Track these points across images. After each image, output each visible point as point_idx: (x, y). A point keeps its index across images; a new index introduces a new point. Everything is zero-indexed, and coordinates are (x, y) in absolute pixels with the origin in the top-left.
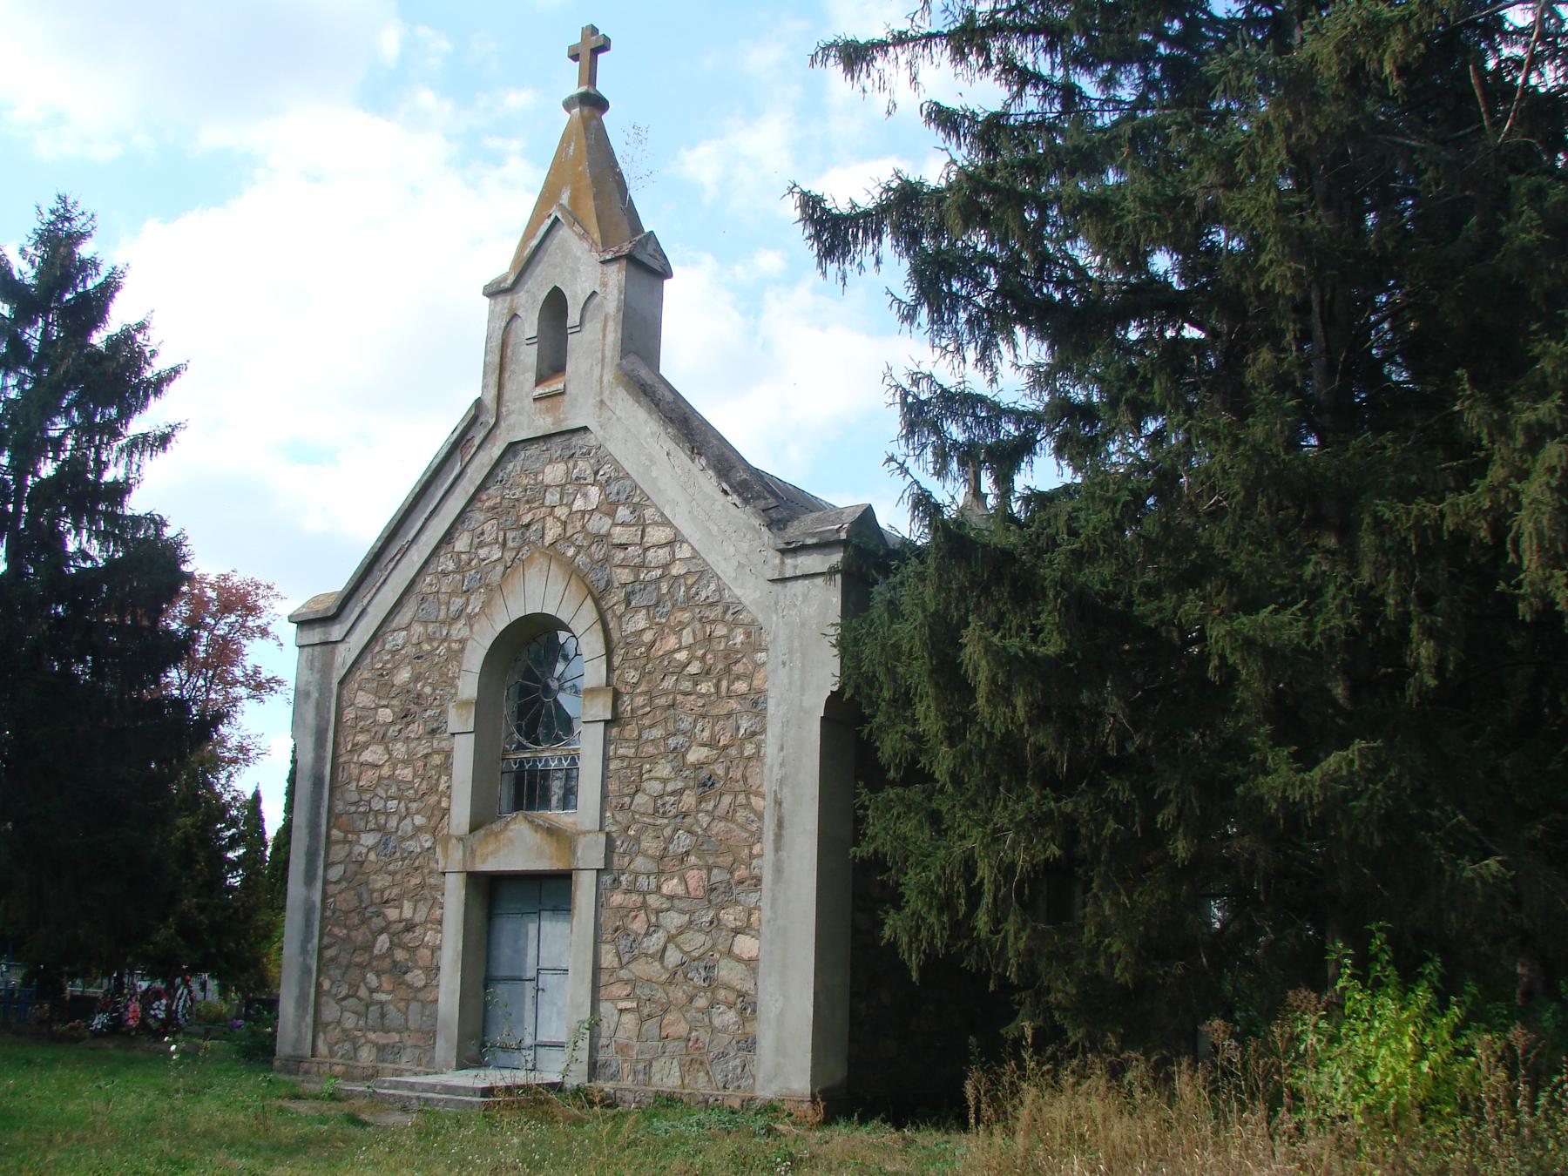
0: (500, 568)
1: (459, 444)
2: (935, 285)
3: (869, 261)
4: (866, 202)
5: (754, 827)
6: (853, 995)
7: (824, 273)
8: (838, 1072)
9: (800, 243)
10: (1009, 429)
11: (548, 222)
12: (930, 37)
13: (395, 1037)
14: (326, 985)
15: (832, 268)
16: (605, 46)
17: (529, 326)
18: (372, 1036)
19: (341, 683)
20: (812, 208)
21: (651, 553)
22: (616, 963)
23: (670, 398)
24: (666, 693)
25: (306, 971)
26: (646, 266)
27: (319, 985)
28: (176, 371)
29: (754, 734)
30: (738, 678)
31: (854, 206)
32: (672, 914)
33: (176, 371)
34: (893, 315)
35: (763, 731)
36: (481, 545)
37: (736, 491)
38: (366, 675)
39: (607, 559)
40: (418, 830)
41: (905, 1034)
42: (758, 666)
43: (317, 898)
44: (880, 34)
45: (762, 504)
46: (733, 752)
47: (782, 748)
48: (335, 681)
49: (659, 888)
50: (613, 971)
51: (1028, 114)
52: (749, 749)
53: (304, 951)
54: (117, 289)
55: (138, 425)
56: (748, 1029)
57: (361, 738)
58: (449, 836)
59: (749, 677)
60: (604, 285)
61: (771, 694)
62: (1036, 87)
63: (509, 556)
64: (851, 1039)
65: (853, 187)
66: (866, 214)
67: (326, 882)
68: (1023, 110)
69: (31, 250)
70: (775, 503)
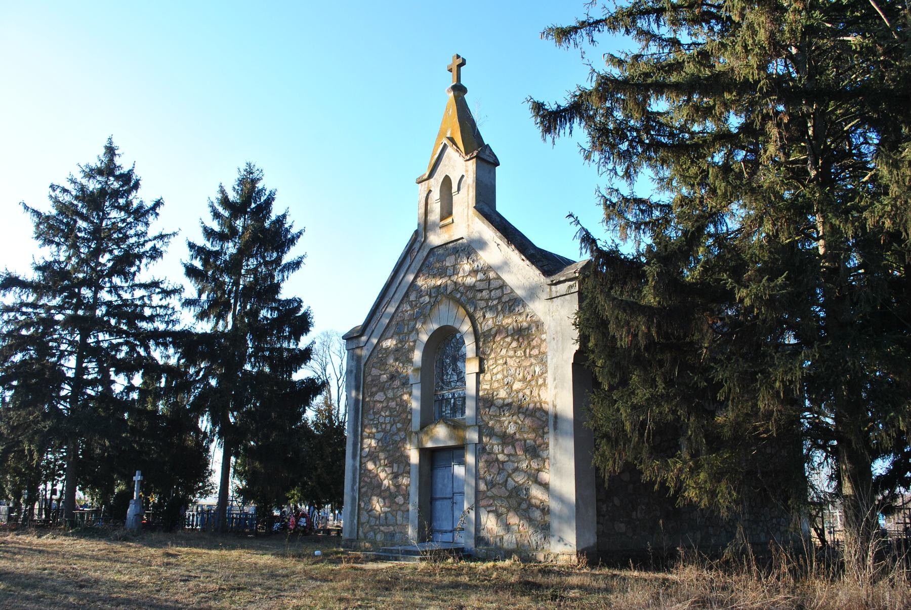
0: (429, 306)
1: (409, 250)
2: (606, 139)
3: (568, 131)
4: (564, 104)
5: (544, 419)
6: (597, 501)
7: (545, 140)
8: (591, 540)
9: (532, 126)
10: (657, 213)
11: (441, 146)
12: (597, 22)
13: (392, 528)
14: (362, 505)
15: (549, 137)
16: (463, 63)
17: (436, 195)
18: (382, 528)
19: (365, 365)
20: (538, 107)
21: (493, 293)
22: (485, 489)
23: (498, 219)
24: (502, 357)
25: (353, 499)
26: (486, 161)
27: (359, 505)
28: (300, 233)
29: (542, 374)
30: (534, 347)
31: (559, 106)
32: (510, 463)
33: (300, 233)
34: (581, 157)
35: (546, 372)
36: (421, 297)
37: (528, 258)
38: (375, 360)
39: (474, 297)
40: (399, 430)
41: (630, 521)
42: (543, 341)
43: (358, 464)
44: (574, 24)
45: (540, 264)
46: (533, 383)
47: (555, 380)
48: (362, 365)
49: (503, 451)
50: (484, 492)
51: (652, 55)
52: (540, 381)
53: (353, 490)
54: (273, 199)
55: (287, 258)
56: (546, 518)
57: (374, 389)
58: (412, 432)
59: (539, 346)
60: (467, 171)
61: (549, 354)
62: (655, 41)
63: (433, 300)
64: (598, 523)
65: (558, 97)
66: (565, 110)
67: (361, 457)
68: (650, 53)
69: (237, 187)
70: (548, 263)
